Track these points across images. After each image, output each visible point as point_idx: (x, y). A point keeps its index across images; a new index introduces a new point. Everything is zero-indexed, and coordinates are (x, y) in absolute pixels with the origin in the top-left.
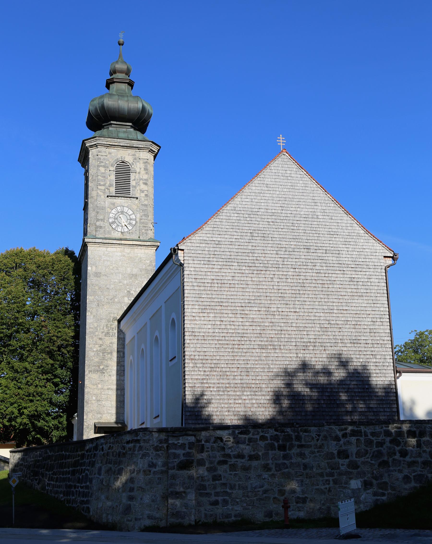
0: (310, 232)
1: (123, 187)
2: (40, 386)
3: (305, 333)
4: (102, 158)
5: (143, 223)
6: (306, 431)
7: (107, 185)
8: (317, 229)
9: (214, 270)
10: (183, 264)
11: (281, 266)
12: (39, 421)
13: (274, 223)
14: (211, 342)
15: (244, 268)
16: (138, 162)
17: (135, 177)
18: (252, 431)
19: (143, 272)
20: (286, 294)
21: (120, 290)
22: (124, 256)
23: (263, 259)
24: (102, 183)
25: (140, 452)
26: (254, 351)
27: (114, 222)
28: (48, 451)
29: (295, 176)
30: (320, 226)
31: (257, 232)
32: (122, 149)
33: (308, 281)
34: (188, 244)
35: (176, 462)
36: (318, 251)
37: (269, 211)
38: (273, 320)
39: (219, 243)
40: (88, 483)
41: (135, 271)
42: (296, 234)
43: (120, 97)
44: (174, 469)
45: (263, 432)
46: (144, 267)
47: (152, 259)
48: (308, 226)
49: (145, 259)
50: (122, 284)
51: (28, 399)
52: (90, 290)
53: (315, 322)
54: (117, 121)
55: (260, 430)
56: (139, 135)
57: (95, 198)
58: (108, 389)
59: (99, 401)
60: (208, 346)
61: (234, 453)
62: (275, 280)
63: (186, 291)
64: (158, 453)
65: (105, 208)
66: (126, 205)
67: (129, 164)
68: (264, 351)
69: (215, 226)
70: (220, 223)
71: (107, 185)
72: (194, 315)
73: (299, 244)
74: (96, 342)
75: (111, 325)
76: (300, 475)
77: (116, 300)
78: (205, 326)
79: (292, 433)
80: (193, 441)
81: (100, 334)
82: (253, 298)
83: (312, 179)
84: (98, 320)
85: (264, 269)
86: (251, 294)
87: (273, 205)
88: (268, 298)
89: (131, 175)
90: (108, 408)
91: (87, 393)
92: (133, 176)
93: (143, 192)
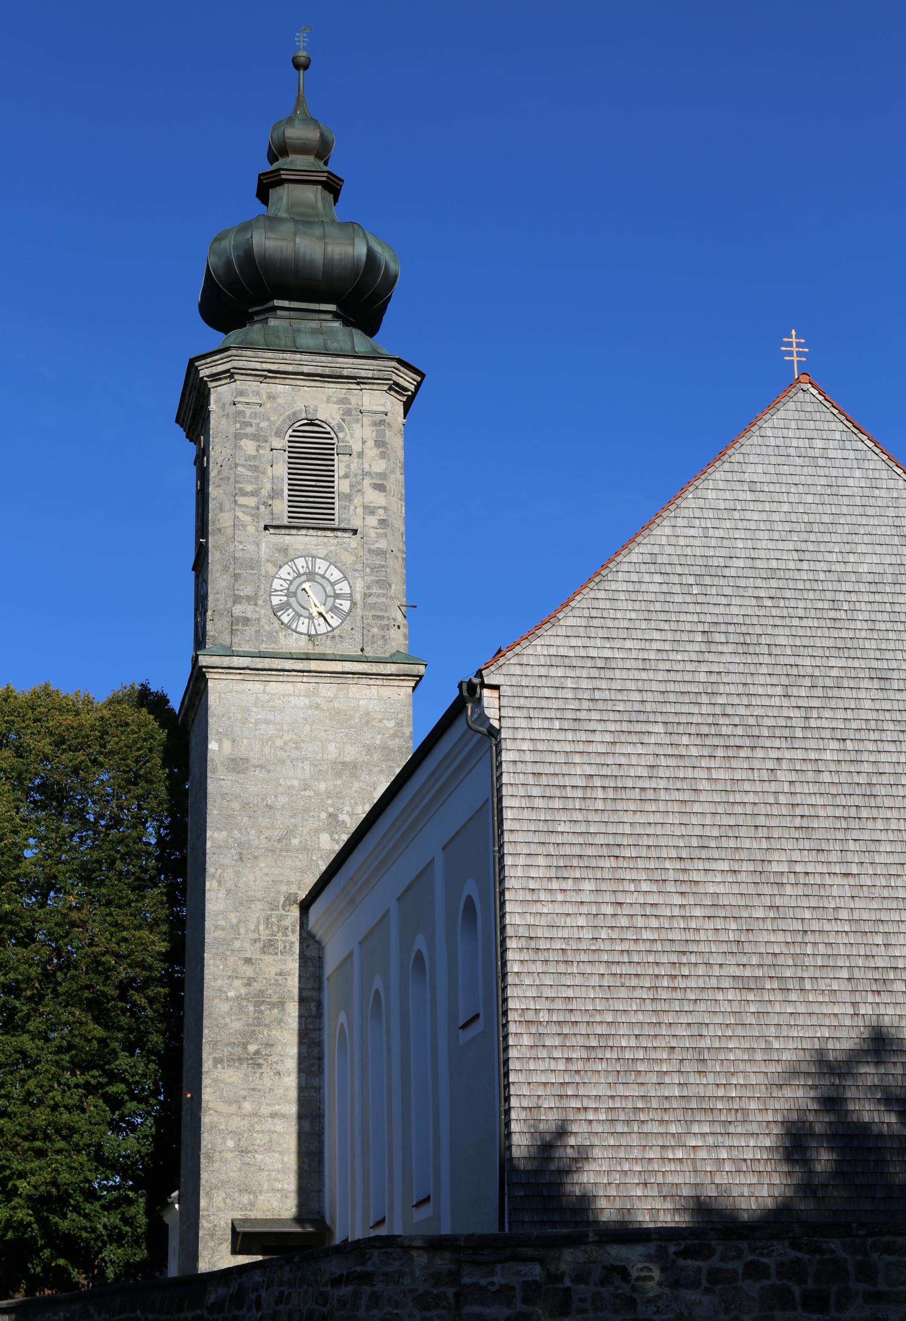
0: (889, 626)
1: (312, 499)
2: (66, 1107)
3: (879, 940)
4: (248, 412)
5: (374, 606)
6: (889, 1249)
7: (264, 492)
9: (591, 748)
11: (799, 733)
14: (588, 969)
15: (685, 740)
16: (357, 421)
18: (719, 1246)
19: (375, 757)
20: (816, 820)
21: (306, 810)
22: (317, 707)
23: (742, 711)
24: (249, 488)
25: (375, 1312)
26: (720, 996)
27: (284, 606)
29: (839, 454)
31: (723, 628)
32: (308, 384)
33: (885, 779)
34: (512, 668)
38: (778, 901)
39: (607, 664)
41: (352, 753)
42: (844, 633)
43: (301, 227)
45: (752, 1250)
46: (378, 742)
47: (401, 716)
49: (379, 716)
51: (29, 1149)
52: (215, 812)
55: (744, 1245)
56: (361, 342)
57: (229, 532)
58: (273, 1115)
59: (244, 1151)
62: (780, 775)
63: (508, 814)
65: (258, 562)
66: (322, 552)
67: (329, 429)
68: (751, 997)
69: (594, 613)
70: (608, 604)
71: (264, 492)
72: (532, 885)
73: (856, 663)
74: (235, 970)
75: (280, 918)
77: (295, 842)
81: (247, 945)
82: (716, 833)
83: (892, 464)
84: (241, 904)
85: (747, 742)
86: (708, 820)
87: (771, 545)
88: (761, 833)
89: (336, 463)
91: (208, 1127)
92: (342, 465)
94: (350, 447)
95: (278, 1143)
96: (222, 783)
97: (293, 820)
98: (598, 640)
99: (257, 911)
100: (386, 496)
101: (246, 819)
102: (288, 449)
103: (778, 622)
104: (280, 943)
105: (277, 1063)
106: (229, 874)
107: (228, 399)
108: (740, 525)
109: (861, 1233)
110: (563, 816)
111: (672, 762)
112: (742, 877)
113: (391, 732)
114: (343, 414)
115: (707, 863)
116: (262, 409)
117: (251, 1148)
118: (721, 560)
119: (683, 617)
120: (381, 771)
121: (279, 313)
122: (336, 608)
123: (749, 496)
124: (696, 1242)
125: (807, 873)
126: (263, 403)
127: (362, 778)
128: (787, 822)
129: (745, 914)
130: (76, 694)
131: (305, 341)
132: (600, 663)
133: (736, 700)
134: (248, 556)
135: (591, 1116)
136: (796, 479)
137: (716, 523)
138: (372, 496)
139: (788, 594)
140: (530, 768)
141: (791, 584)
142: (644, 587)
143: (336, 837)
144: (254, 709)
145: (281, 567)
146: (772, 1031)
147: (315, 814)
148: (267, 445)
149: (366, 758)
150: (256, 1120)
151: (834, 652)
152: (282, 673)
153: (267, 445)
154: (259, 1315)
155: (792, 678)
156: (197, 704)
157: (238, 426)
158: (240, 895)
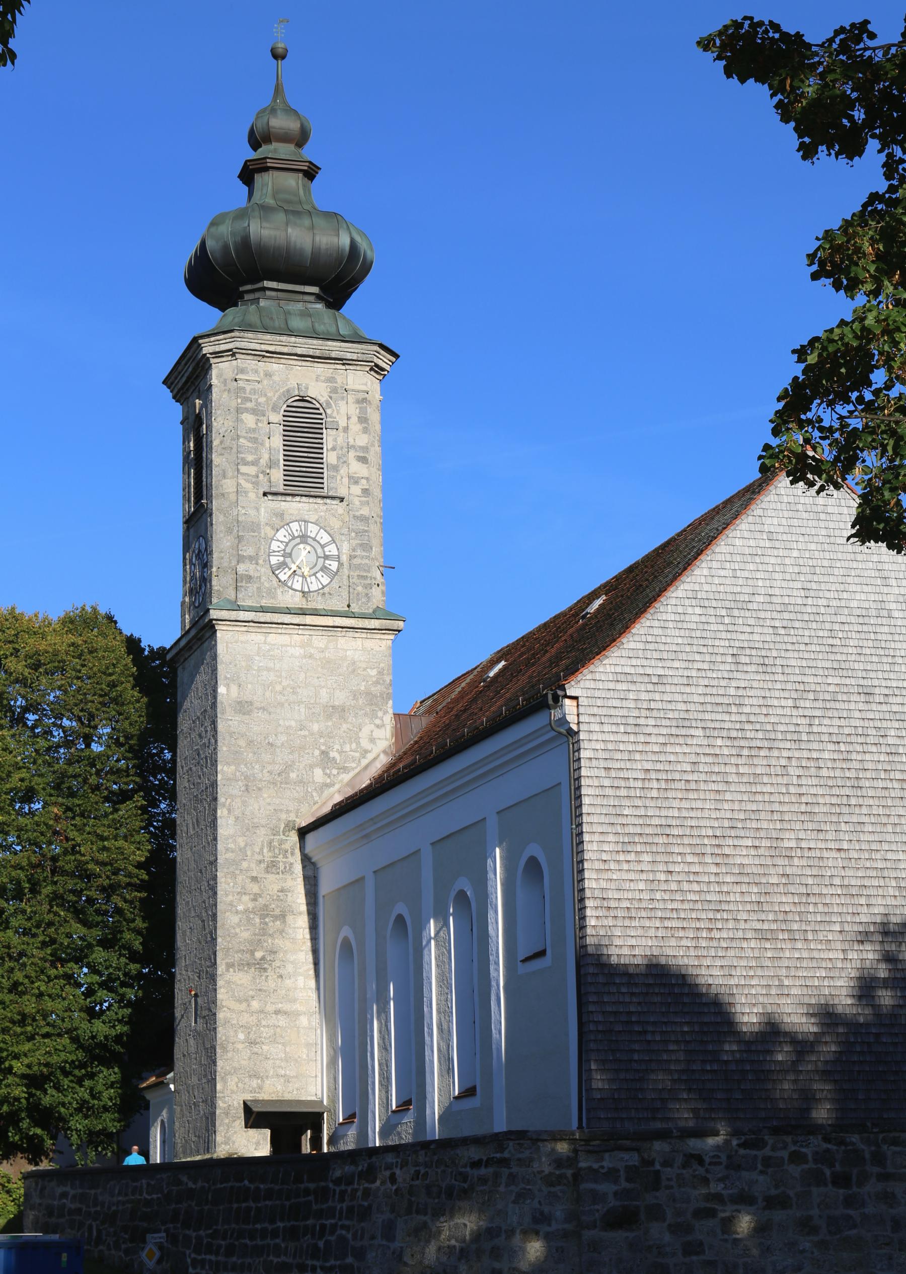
0: (873, 651)
1: (304, 470)
2: (50, 996)
3: (863, 901)
4: (248, 388)
5: (359, 567)
6: (895, 1142)
7: (263, 462)
8: (888, 645)
9: (648, 748)
10: (577, 733)
11: (804, 737)
12: (45, 1092)
13: (787, 631)
14: (647, 923)
15: (719, 742)
16: (343, 398)
17: (335, 440)
18: (770, 1140)
19: (360, 702)
20: (817, 806)
21: (302, 748)
22: (311, 656)
23: (762, 719)
24: (250, 458)
25: (512, 1188)
26: (745, 945)
27: (283, 565)
28: (185, 1179)
29: (836, 510)
30: (896, 638)
31: (748, 652)
32: (300, 363)
33: (868, 775)
34: (587, 682)
35: (598, 1211)
36: (891, 700)
37: (774, 599)
38: (789, 871)
39: (661, 680)
40: (349, 1260)
41: (341, 697)
42: (839, 657)
43: (291, 217)
44: (595, 1227)
45: (795, 1143)
46: (363, 688)
47: (382, 665)
48: (867, 636)
49: (364, 665)
50: (307, 733)
51: (22, 1034)
52: (225, 749)
53: (886, 874)
54: (279, 281)
55: (788, 1139)
57: (233, 497)
58: (277, 1012)
59: (253, 1043)
60: (640, 932)
61: (731, 1192)
63: (586, 800)
64: (552, 1189)
65: (259, 525)
67: (318, 406)
68: (768, 945)
69: (650, 639)
70: (660, 632)
71: (263, 462)
72: (605, 857)
73: (848, 681)
74: (243, 887)
75: (281, 842)
76: (886, 1244)
77: (293, 775)
78: (632, 884)
79: (862, 1146)
80: (636, 1163)
81: (253, 866)
82: (742, 816)
84: (248, 830)
85: (766, 744)
86: (736, 806)
87: (784, 584)
88: (776, 816)
89: (324, 436)
90: (278, 1062)
91: (222, 1022)
93: (356, 483)
94: (337, 422)
95: (281, 1036)
96: (230, 722)
97: (291, 757)
98: (653, 661)
99: (262, 835)
100: (368, 468)
101: (251, 755)
102: (282, 423)
103: (789, 647)
104: (281, 864)
105: (279, 967)
106: (237, 804)
107: (230, 375)
108: (760, 567)
109: (875, 1130)
110: (626, 802)
111: (710, 759)
112: (761, 851)
113: (374, 679)
114: (330, 392)
115: (735, 840)
116: (260, 386)
117: (258, 1040)
118: (746, 596)
119: (717, 643)
120: (366, 714)
121: (268, 293)
122: (326, 567)
123: (768, 544)
124: (753, 1136)
125: (810, 849)
126: (260, 378)
127: (350, 720)
128: (795, 808)
129: (764, 881)
130: (36, 616)
131: (296, 323)
132: (655, 680)
133: (757, 711)
134: (249, 519)
135: (649, 1037)
136: (803, 531)
137: (742, 566)
138: (357, 468)
139: (797, 624)
140: (602, 764)
141: (799, 617)
142: (687, 618)
143: (328, 771)
144: (257, 658)
145: (278, 530)
146: (784, 972)
147: (310, 751)
148: (265, 419)
149: (353, 703)
150: (262, 1016)
151: (832, 672)
152: (281, 626)
153: (265, 419)
154: (394, 1187)
155: (799, 693)
156: (195, 648)
157: (239, 401)
158: (247, 821)
